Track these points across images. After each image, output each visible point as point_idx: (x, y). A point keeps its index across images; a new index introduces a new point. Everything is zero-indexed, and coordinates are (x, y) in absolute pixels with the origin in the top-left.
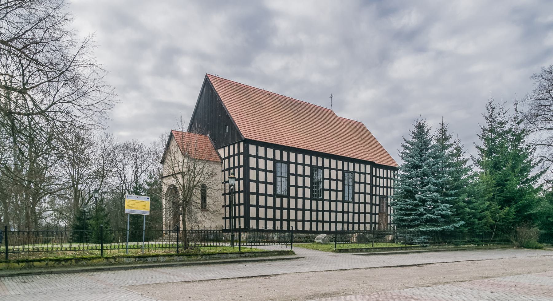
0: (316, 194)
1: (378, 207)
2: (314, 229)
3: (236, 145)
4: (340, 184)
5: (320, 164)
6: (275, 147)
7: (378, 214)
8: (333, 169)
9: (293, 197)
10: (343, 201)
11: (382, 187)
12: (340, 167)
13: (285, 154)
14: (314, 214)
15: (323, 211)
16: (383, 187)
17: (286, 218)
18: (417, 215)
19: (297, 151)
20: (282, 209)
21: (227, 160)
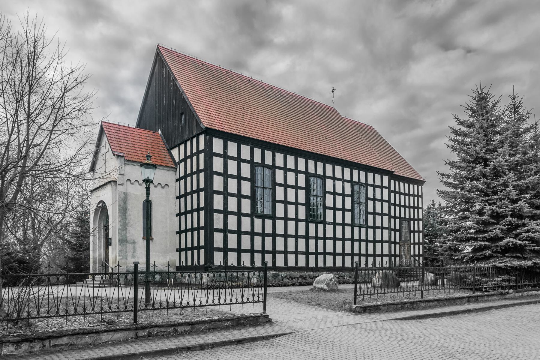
0: (315, 217)
1: (398, 233)
2: (312, 264)
3: (195, 140)
4: (348, 200)
5: (320, 172)
6: (254, 143)
7: (398, 243)
8: (338, 179)
9: (280, 218)
10: (353, 225)
11: (403, 206)
12: (347, 177)
13: (268, 154)
14: (312, 242)
15: (325, 238)
16: (405, 206)
17: (271, 249)
18: (488, 240)
19: (287, 151)
20: (263, 235)
21: (182, 165)
